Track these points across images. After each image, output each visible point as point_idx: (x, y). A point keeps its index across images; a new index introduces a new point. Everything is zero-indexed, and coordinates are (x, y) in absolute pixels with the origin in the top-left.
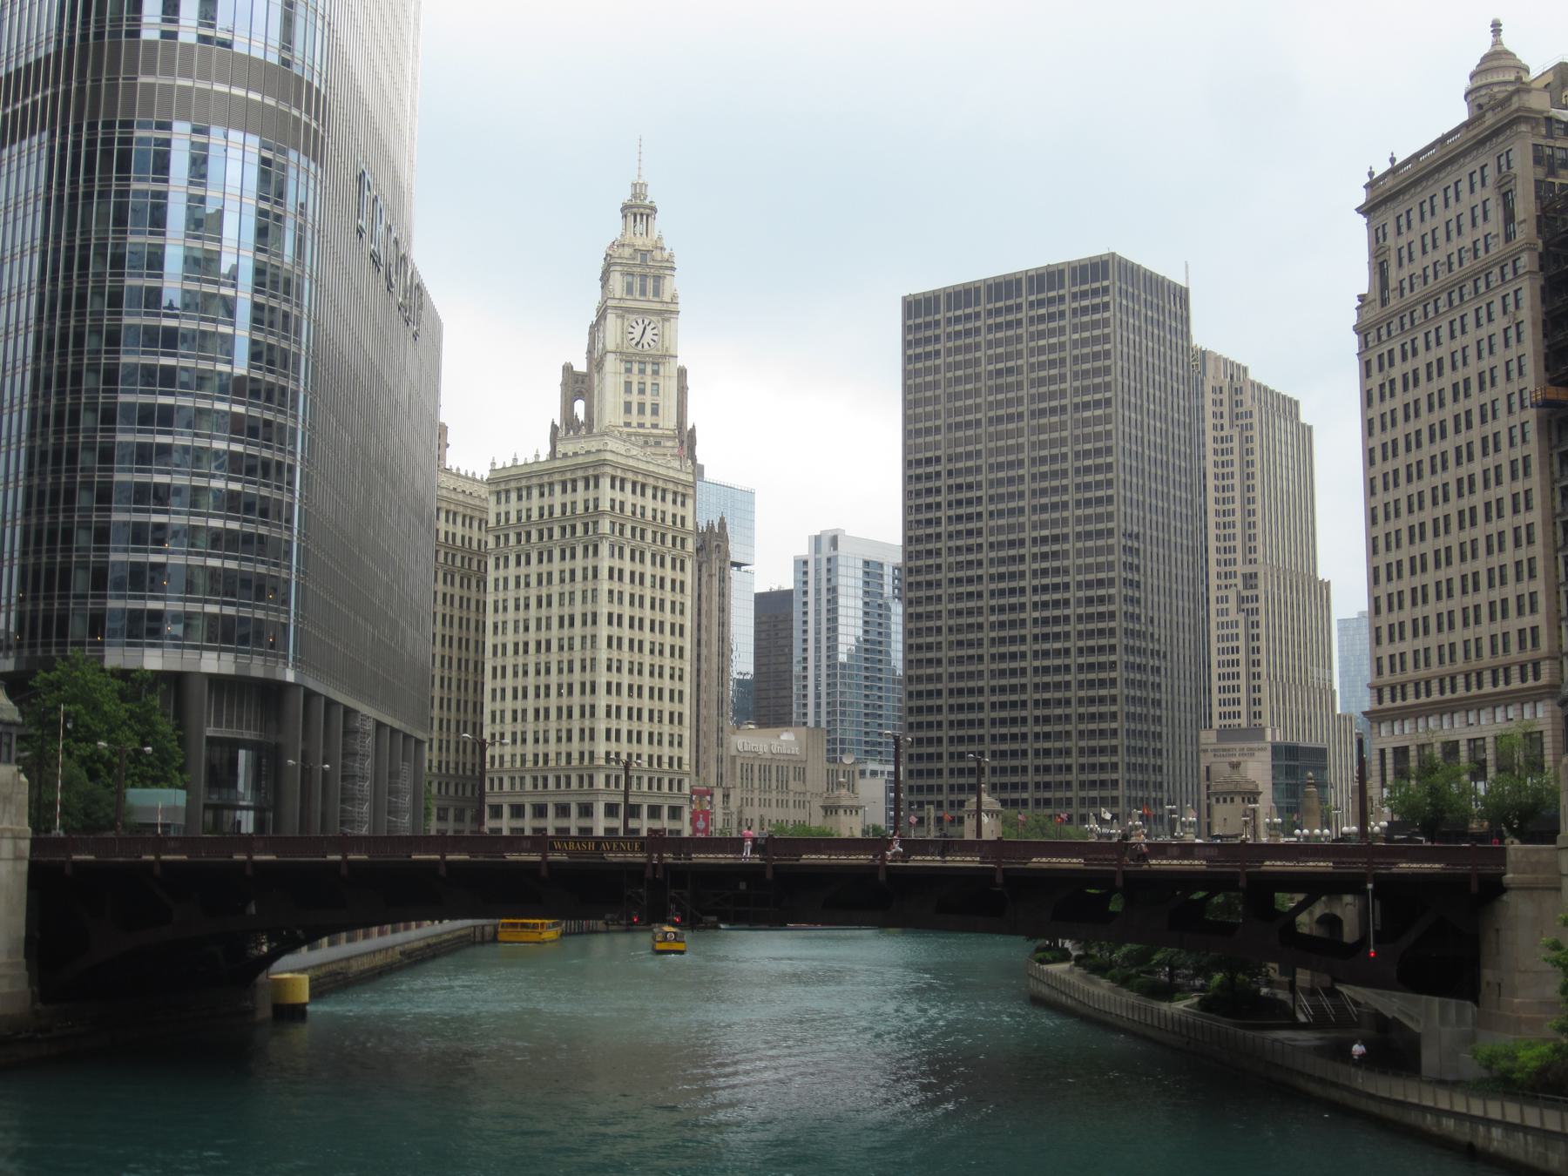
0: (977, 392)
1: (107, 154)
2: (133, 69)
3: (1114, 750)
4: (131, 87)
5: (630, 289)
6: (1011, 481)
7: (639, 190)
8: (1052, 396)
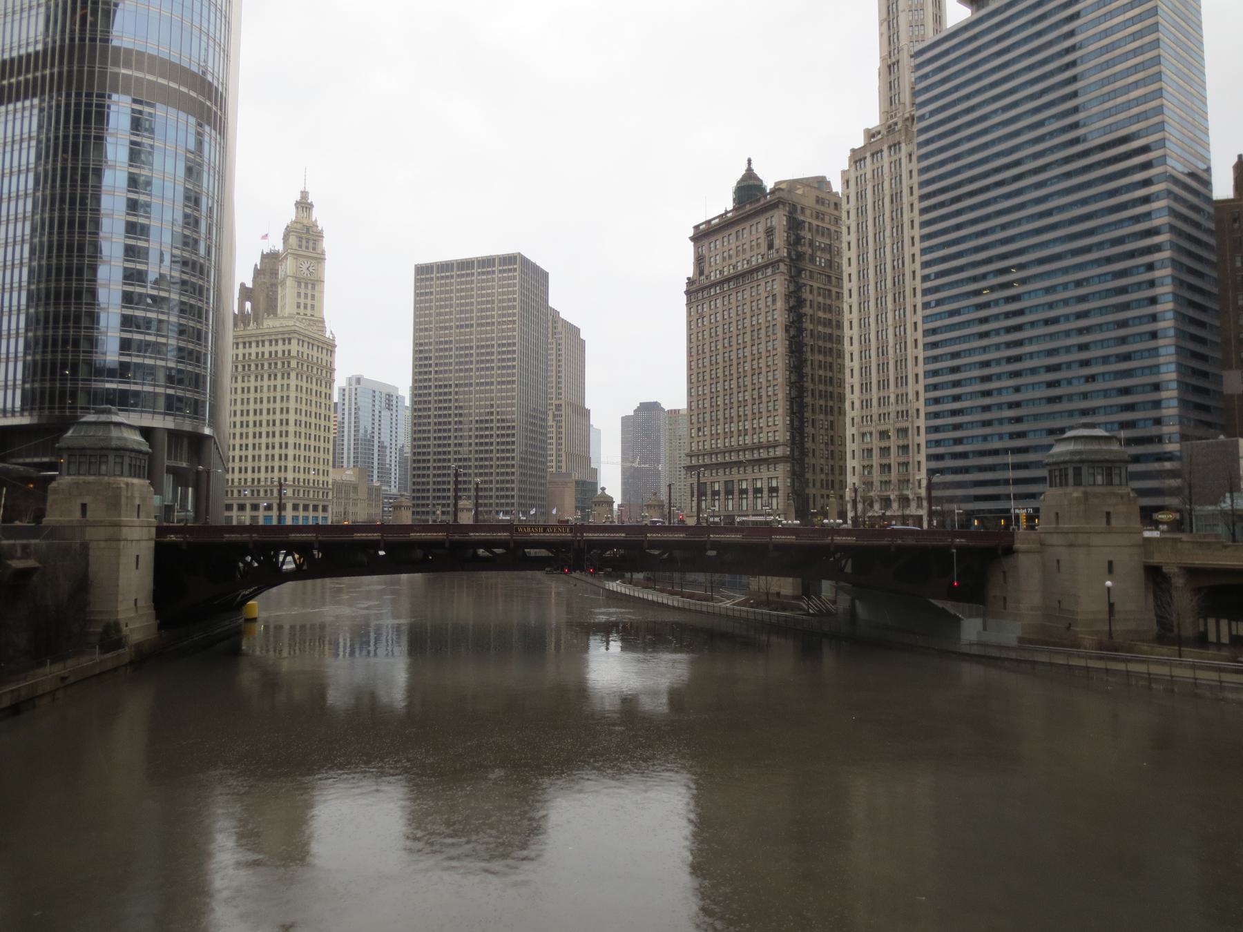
0: (451, 313)
1: (88, 114)
2: (104, 61)
3: (513, 482)
4: (103, 74)
5: (300, 246)
6: (466, 355)
7: (304, 194)
8: (487, 317)
